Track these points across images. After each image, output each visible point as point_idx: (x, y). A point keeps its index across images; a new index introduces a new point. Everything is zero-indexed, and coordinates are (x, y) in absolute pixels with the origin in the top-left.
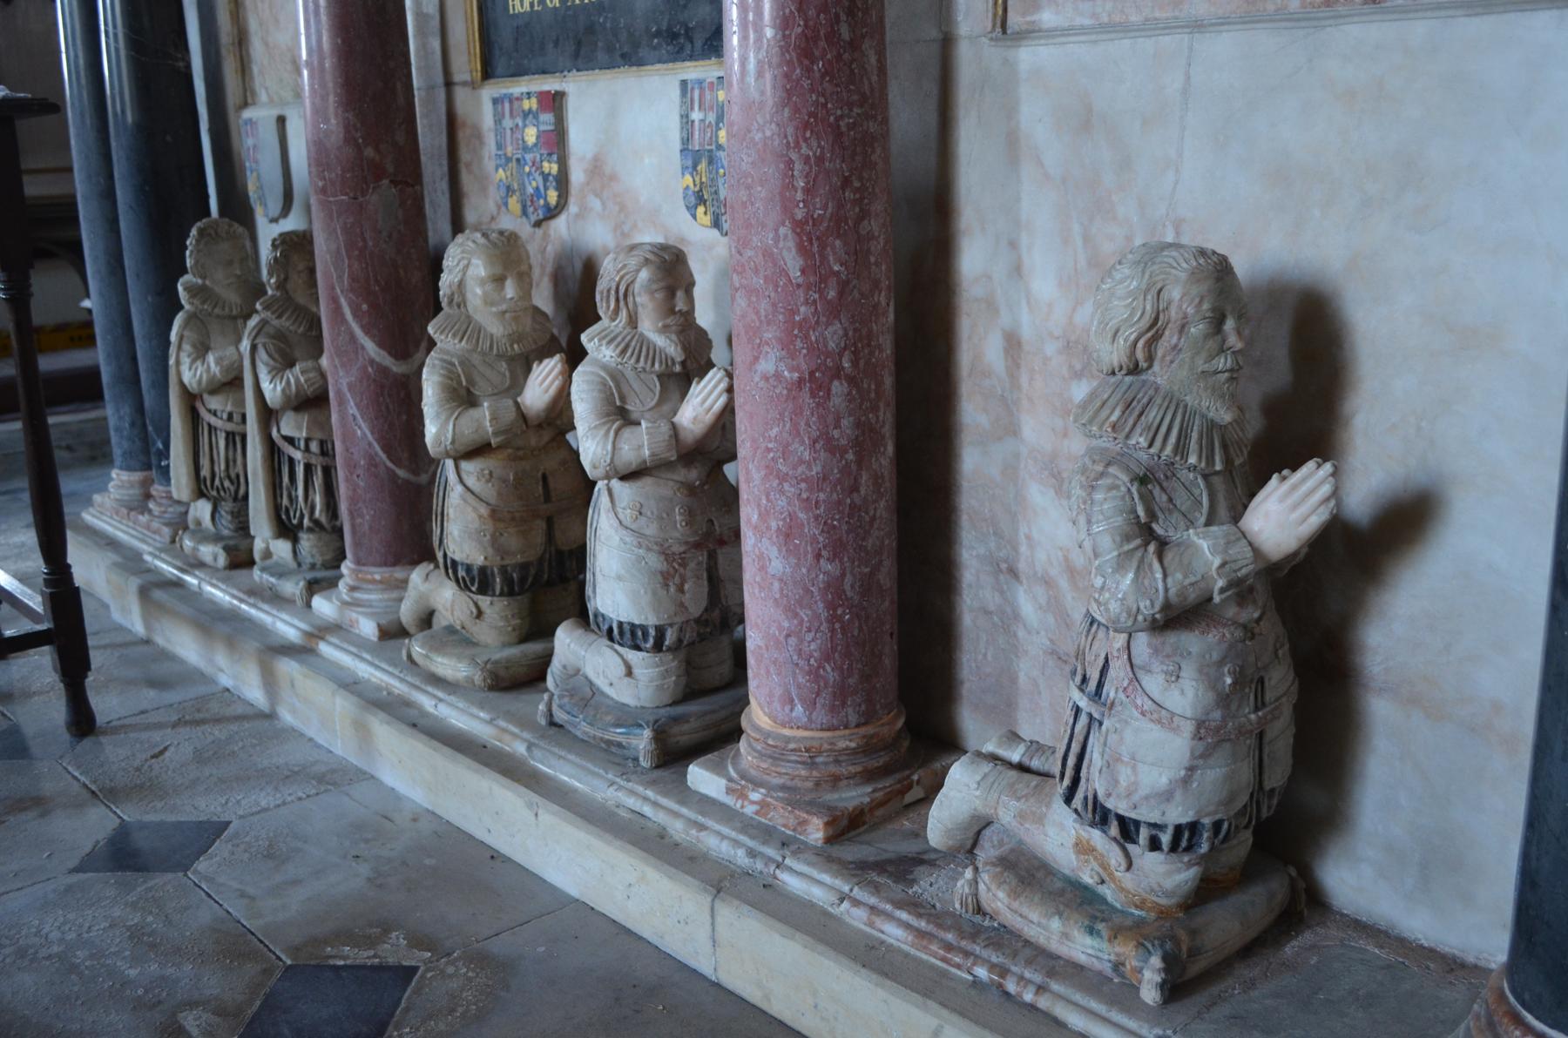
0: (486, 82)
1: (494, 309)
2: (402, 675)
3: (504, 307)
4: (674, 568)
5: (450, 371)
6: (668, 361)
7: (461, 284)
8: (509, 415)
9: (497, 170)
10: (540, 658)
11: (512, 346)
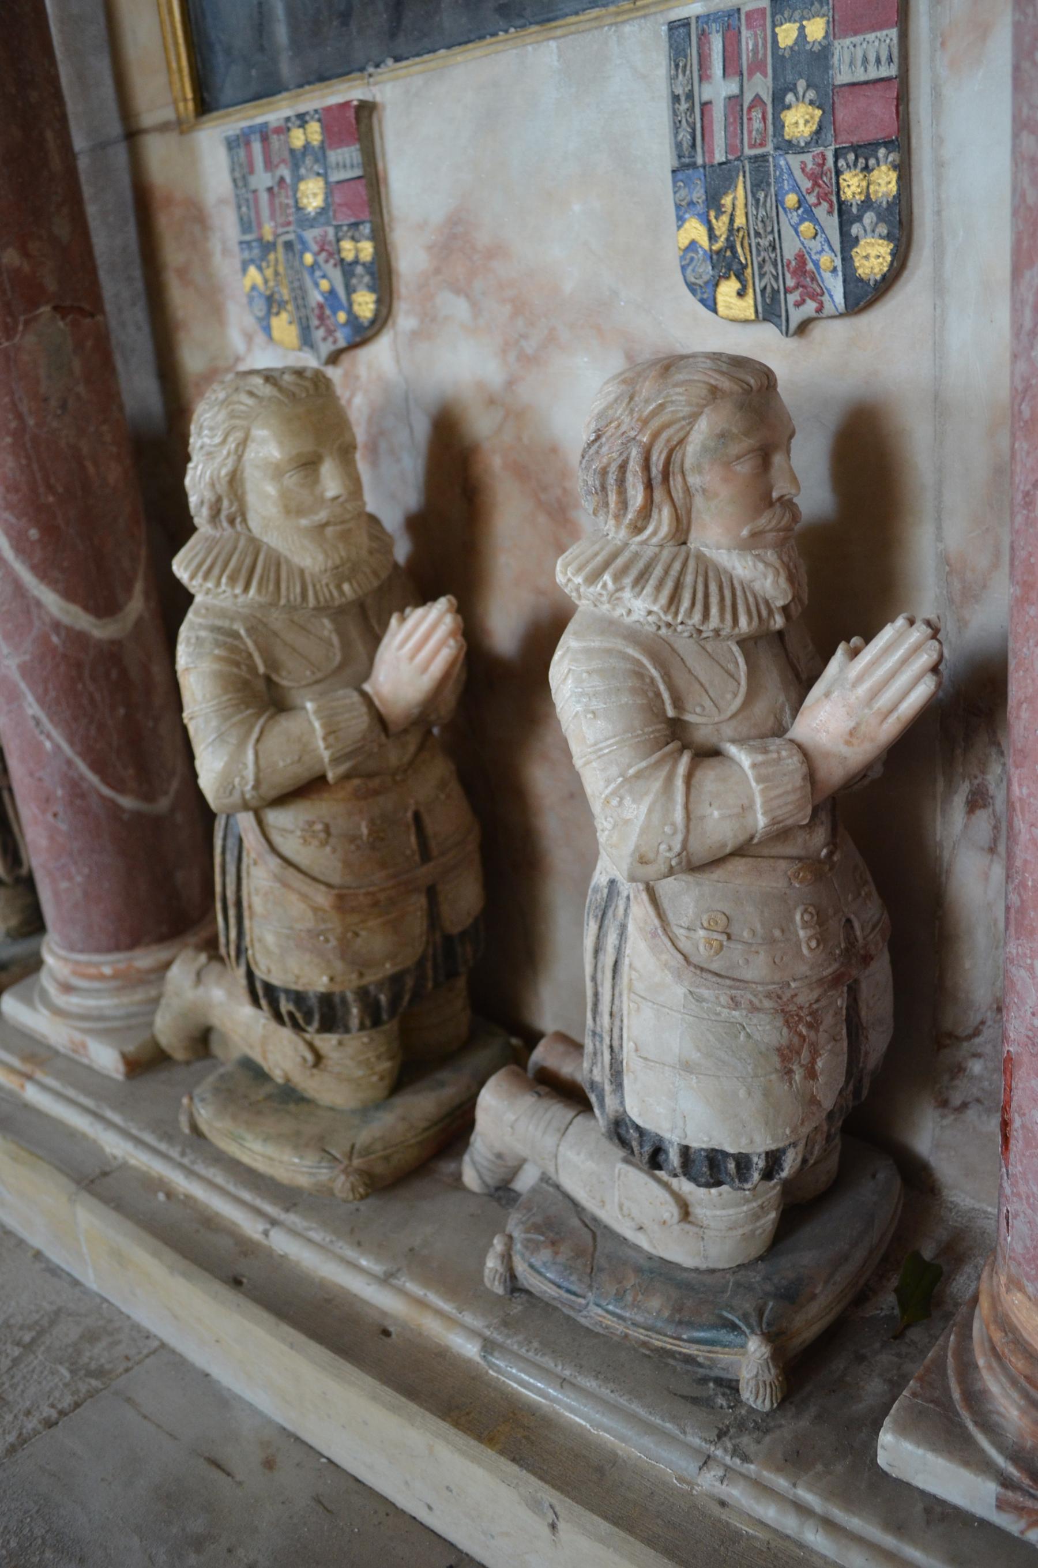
0: (205, 118)
1: (304, 522)
2: (186, 1161)
3: (322, 516)
4: (800, 1035)
5: (233, 649)
6: (760, 608)
7: (235, 479)
8: (359, 722)
9: (244, 270)
10: (435, 1124)
11: (339, 587)
